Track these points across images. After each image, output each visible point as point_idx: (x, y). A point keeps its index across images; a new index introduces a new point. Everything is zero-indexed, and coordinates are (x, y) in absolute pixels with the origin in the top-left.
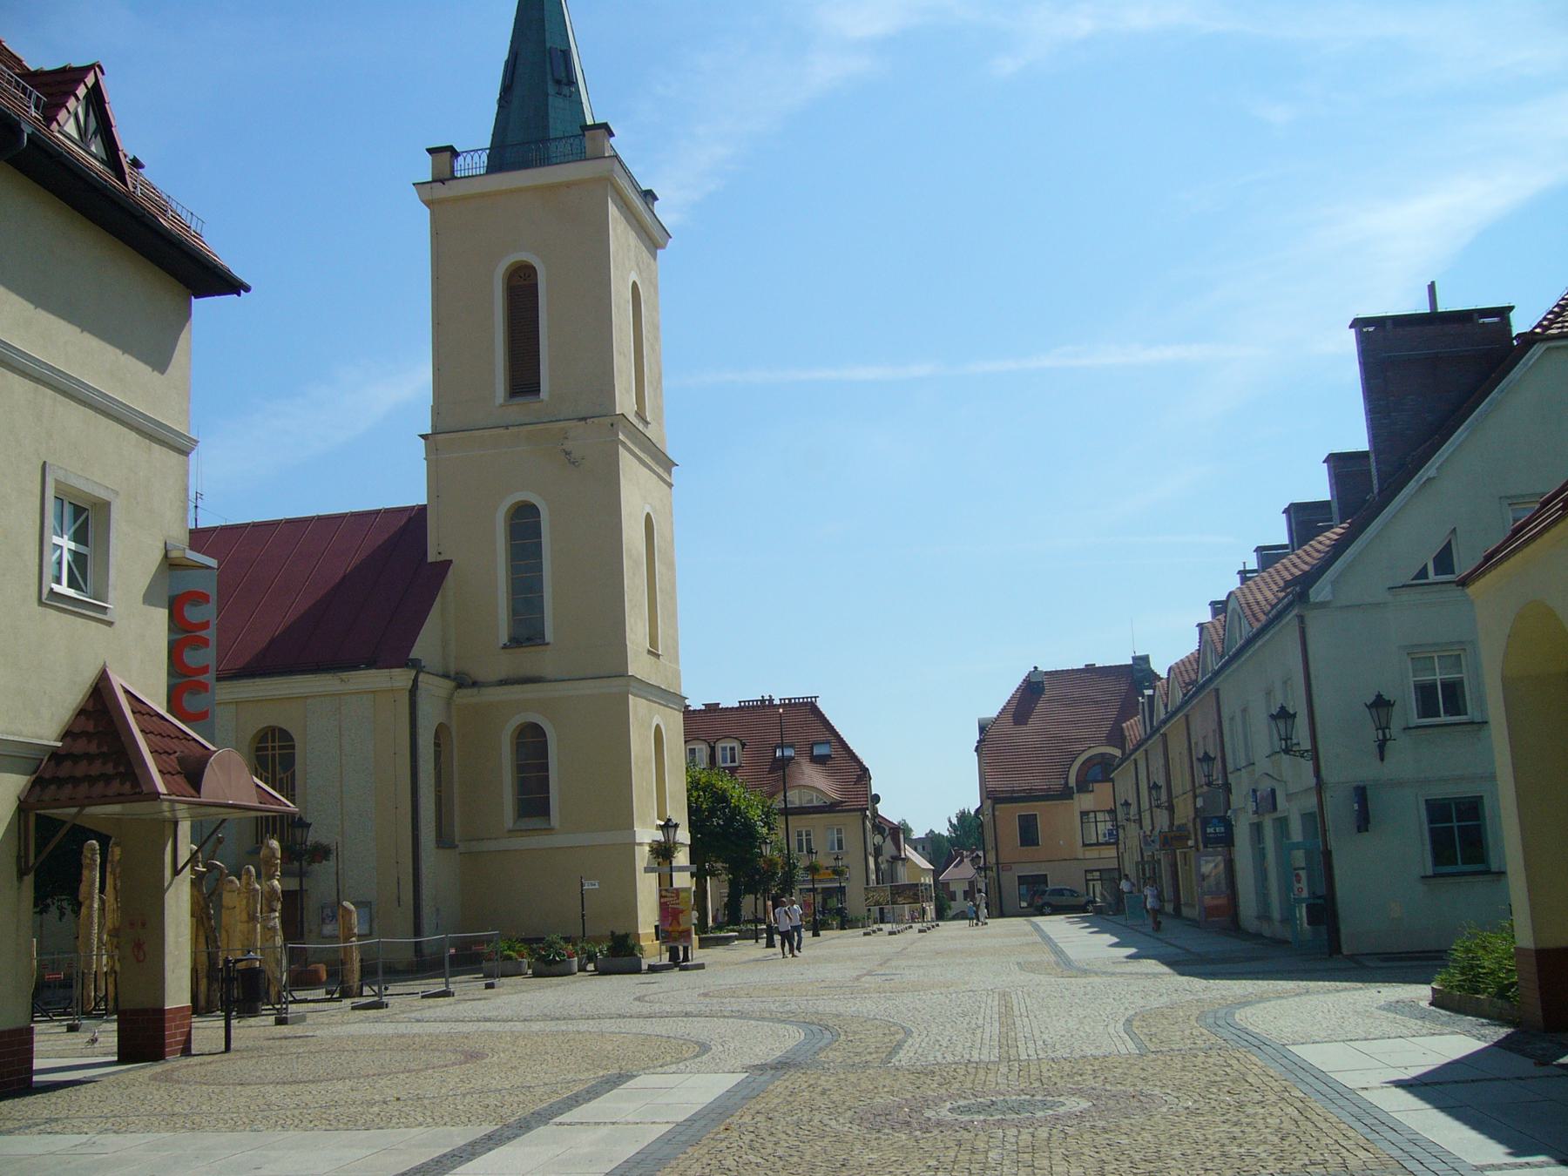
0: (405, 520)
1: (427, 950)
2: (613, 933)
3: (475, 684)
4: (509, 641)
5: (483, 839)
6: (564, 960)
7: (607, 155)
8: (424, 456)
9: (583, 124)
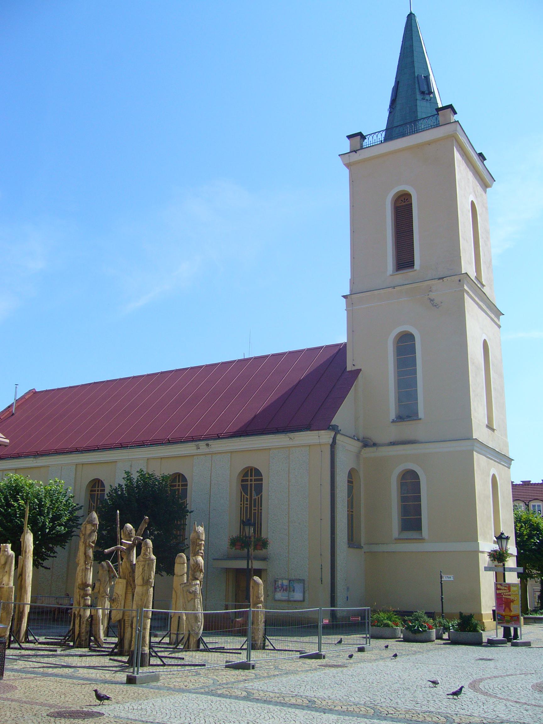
0: (337, 350)
1: (339, 615)
2: (461, 614)
3: (375, 445)
4: (397, 418)
5: (379, 544)
6: (425, 631)
7: (452, 122)
8: (345, 308)
9: (437, 108)
